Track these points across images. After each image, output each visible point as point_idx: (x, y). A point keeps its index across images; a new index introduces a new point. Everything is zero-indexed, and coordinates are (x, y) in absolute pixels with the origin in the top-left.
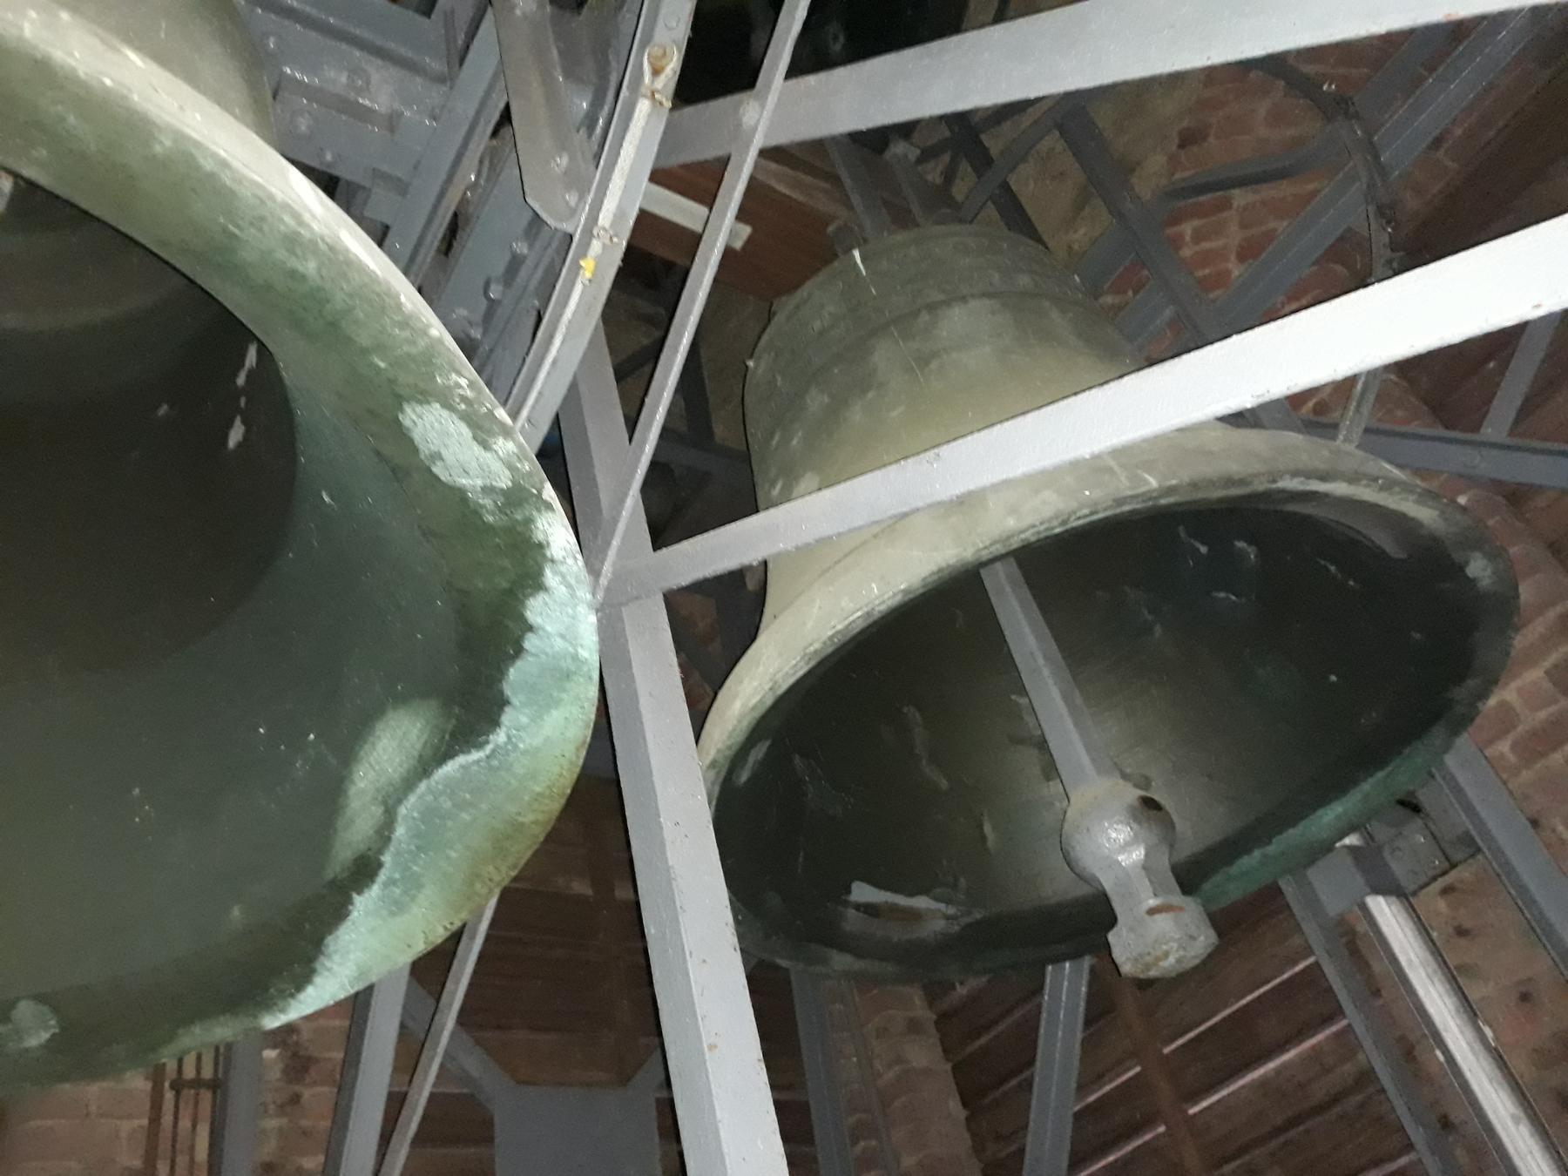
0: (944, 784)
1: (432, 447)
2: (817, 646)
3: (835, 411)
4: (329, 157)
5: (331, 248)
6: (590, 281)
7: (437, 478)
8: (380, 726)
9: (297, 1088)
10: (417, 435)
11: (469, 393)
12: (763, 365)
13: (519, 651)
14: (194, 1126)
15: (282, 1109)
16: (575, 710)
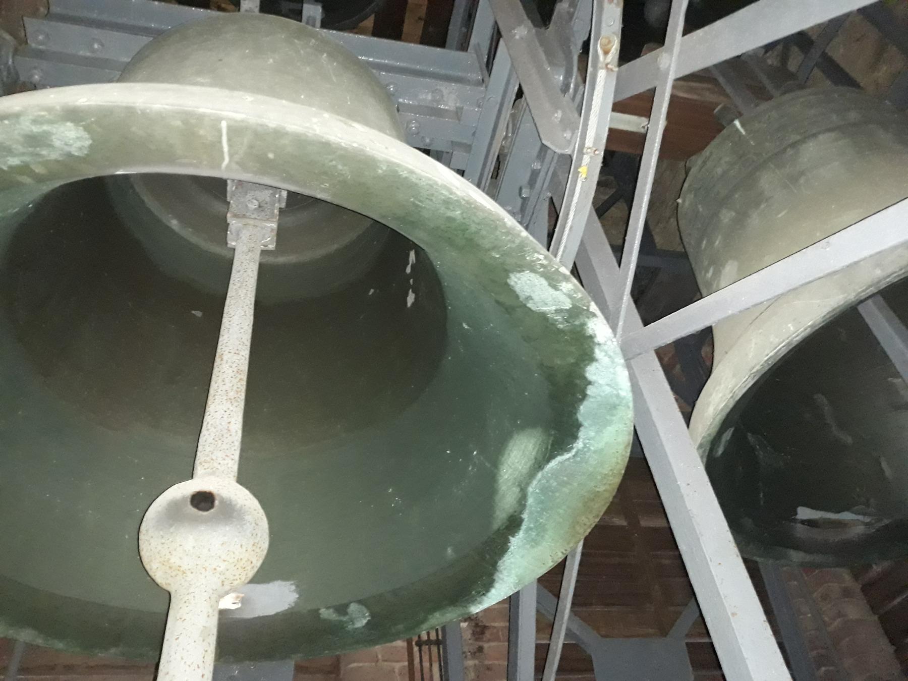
0: (849, 440)
1: (526, 293)
2: (758, 367)
3: (741, 220)
4: (428, 141)
5: (468, 202)
6: (585, 178)
7: (530, 309)
8: (511, 444)
9: (481, 644)
10: (518, 289)
11: (545, 262)
12: (687, 203)
13: (585, 396)
14: (431, 665)
15: (474, 654)
16: (621, 426)
